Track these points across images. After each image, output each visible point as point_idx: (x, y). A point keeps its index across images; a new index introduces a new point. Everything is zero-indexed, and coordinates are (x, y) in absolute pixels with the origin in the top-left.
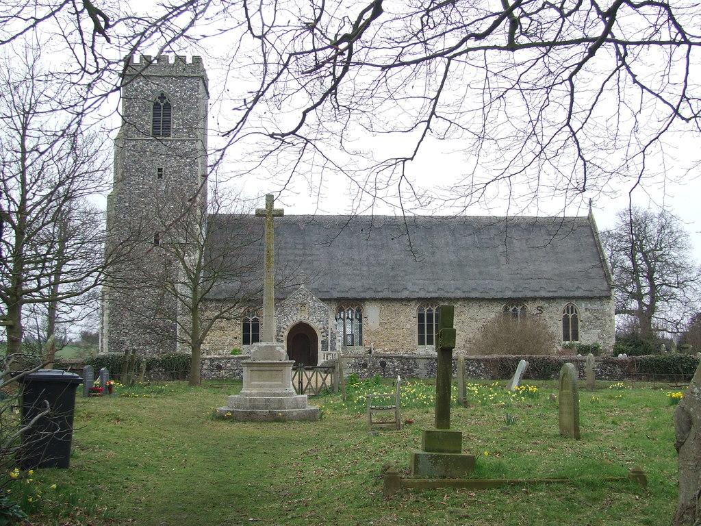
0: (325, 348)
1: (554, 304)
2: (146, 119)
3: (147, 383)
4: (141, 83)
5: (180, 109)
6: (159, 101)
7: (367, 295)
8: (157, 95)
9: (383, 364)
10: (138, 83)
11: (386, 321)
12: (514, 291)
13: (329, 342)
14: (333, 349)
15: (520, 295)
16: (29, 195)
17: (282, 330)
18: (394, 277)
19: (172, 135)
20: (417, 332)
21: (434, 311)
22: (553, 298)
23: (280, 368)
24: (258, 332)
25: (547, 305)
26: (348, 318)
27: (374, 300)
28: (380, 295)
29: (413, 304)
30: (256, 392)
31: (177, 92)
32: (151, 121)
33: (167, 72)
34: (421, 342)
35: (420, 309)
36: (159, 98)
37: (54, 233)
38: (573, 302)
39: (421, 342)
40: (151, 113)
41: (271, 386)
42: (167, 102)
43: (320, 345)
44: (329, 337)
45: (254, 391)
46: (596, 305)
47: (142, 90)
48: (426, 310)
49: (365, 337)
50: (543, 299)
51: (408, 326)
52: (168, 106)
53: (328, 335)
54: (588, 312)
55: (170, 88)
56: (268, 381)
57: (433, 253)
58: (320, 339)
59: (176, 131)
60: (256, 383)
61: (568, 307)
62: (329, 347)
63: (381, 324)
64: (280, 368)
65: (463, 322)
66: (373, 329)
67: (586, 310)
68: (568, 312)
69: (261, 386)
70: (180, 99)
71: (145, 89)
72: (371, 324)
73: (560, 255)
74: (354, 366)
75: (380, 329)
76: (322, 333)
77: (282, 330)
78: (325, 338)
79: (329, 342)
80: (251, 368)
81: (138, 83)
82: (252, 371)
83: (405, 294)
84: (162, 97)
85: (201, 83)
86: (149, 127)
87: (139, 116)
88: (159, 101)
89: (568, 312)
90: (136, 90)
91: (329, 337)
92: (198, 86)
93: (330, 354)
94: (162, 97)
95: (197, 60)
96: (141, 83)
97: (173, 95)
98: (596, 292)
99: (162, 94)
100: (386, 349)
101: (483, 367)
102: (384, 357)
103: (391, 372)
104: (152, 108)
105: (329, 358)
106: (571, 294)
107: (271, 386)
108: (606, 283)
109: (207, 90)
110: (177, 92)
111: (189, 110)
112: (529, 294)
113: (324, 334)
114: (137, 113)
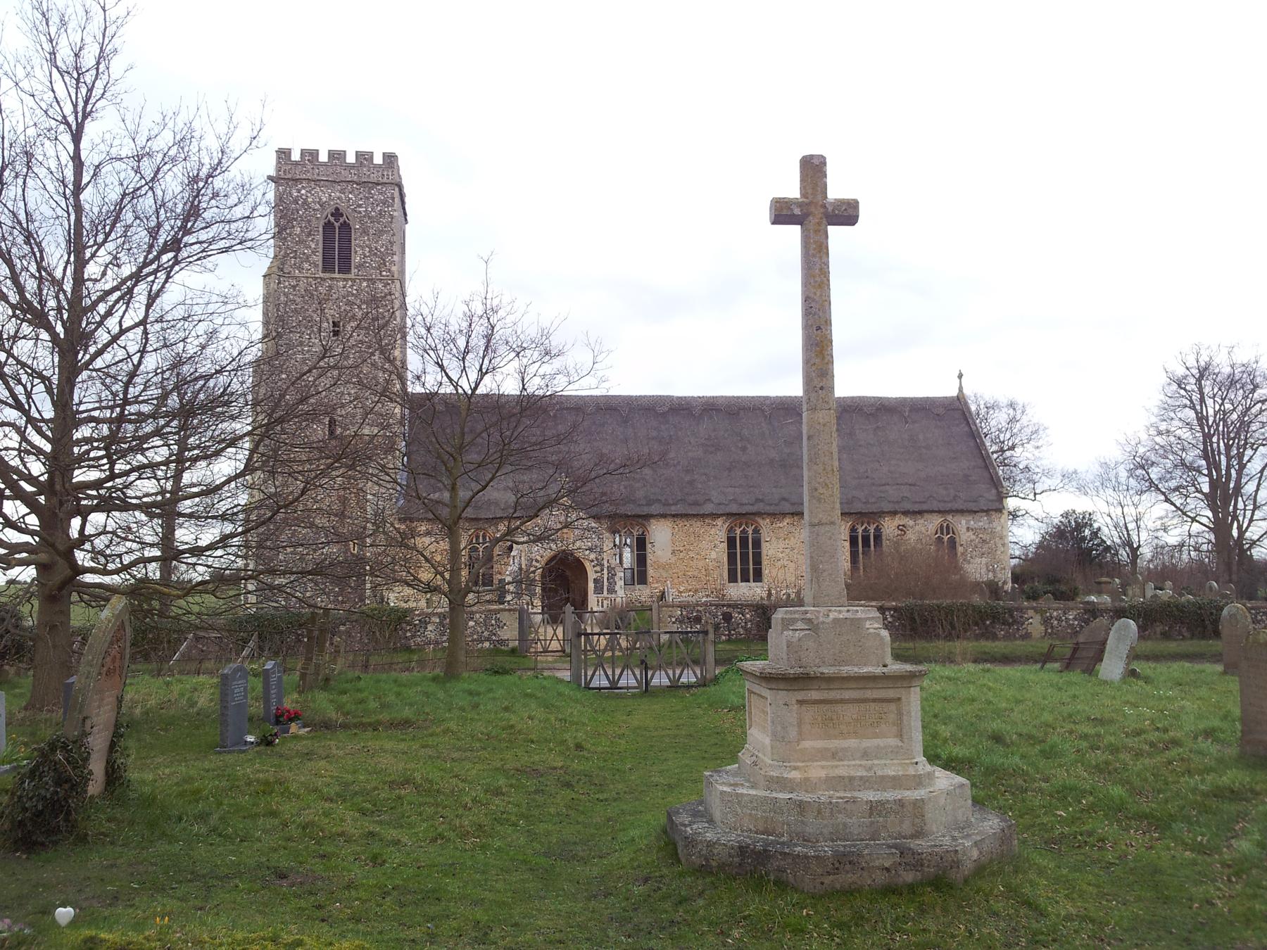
0: (599, 590)
1: (921, 521)
2: (313, 246)
3: (504, 816)
4: (303, 192)
5: (365, 232)
6: (332, 219)
7: (655, 509)
8: (330, 210)
9: (727, 617)
10: (299, 191)
11: (682, 549)
12: (864, 503)
13: (605, 580)
14: (612, 590)
15: (874, 508)
16: (92, 270)
17: (534, 563)
18: (691, 483)
19: (354, 271)
20: (726, 563)
21: (751, 532)
22: (920, 513)
23: (891, 694)
24: (645, 566)
25: (911, 523)
26: (626, 544)
27: (664, 516)
28: (673, 510)
29: (719, 522)
30: (823, 774)
31: (360, 206)
32: (321, 250)
33: (346, 175)
34: (732, 578)
35: (731, 530)
36: (332, 215)
37: (64, 117)
38: (950, 518)
39: (732, 578)
40: (320, 237)
41: (865, 755)
42: (345, 222)
43: (591, 585)
44: (605, 571)
45: (817, 771)
46: (982, 522)
47: (305, 202)
48: (738, 532)
49: (651, 572)
50: (906, 513)
51: (714, 555)
52: (346, 227)
53: (602, 570)
54: (971, 533)
55: (348, 200)
56: (856, 734)
57: (744, 449)
58: (592, 576)
59: (360, 266)
60: (820, 744)
61: (942, 527)
62: (605, 588)
63: (673, 552)
64: (891, 694)
65: (793, 549)
66: (663, 560)
67: (968, 529)
68: (942, 534)
69: (834, 755)
70: (364, 216)
71: (310, 200)
72: (659, 553)
73: (924, 451)
74: (680, 621)
75: (674, 559)
76: (594, 566)
77: (534, 563)
78: (599, 574)
79: (605, 580)
80: (801, 695)
81: (299, 191)
82: (801, 702)
83: (708, 508)
84: (337, 213)
85: (397, 189)
86: (318, 258)
87: (301, 242)
88: (332, 219)
89: (942, 534)
90: (296, 202)
91: (605, 571)
92: (393, 199)
93: (607, 598)
94: (337, 213)
95: (390, 159)
96: (303, 192)
97: (354, 210)
98: (983, 504)
99: (337, 209)
100: (682, 589)
101: (889, 620)
102: (729, 606)
103: (742, 631)
104: (321, 229)
105: (605, 606)
106: (948, 506)
107: (865, 755)
108: (994, 491)
109: (404, 209)
110: (360, 206)
111: (380, 233)
112: (887, 507)
113: (598, 568)
114: (298, 237)
